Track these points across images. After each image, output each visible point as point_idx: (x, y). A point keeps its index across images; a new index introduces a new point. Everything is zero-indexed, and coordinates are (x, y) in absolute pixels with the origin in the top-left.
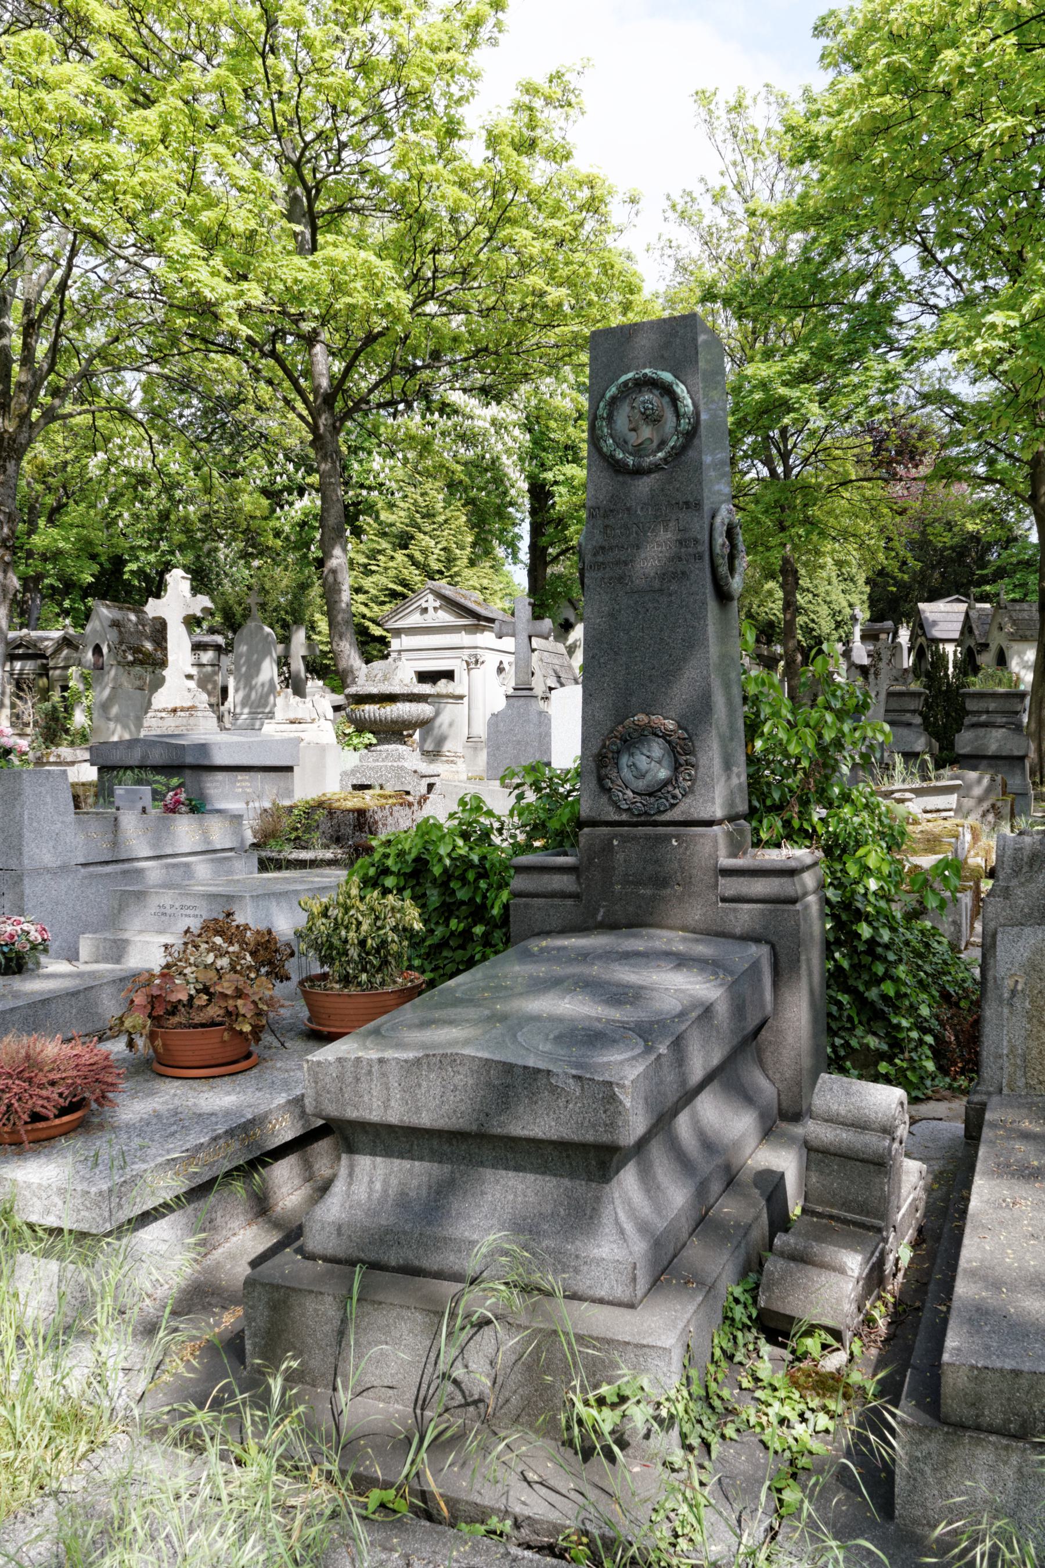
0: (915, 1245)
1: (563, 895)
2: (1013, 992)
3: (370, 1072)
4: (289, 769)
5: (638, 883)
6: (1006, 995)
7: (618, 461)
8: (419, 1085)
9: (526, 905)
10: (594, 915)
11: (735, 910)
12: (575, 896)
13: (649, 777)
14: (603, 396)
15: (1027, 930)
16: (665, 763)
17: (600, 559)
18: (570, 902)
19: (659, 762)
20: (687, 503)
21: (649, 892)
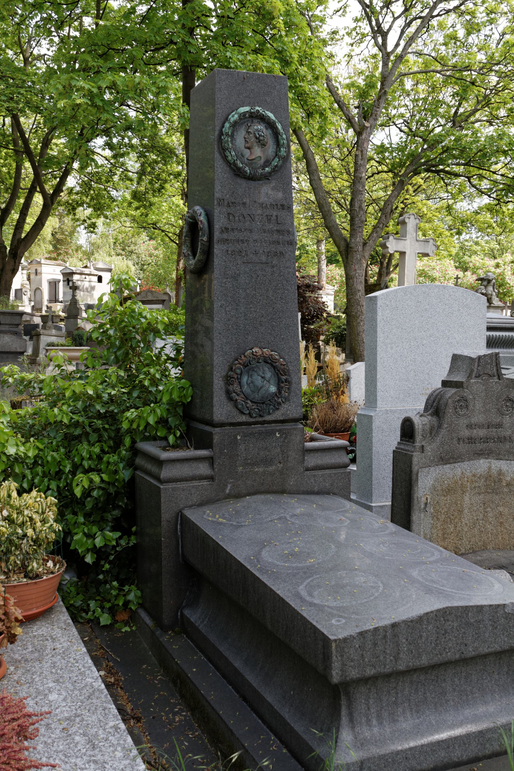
0: (236, 669)
1: (201, 478)
2: (426, 504)
3: (385, 637)
4: (423, 452)
5: (253, 465)
6: (423, 506)
7: (239, 169)
8: (421, 636)
9: (173, 489)
10: (224, 490)
11: (314, 476)
12: (211, 478)
13: (262, 391)
14: (226, 119)
15: (432, 469)
16: (272, 381)
17: (225, 236)
18: (205, 483)
19: (269, 381)
20: (282, 205)
21: (261, 470)
